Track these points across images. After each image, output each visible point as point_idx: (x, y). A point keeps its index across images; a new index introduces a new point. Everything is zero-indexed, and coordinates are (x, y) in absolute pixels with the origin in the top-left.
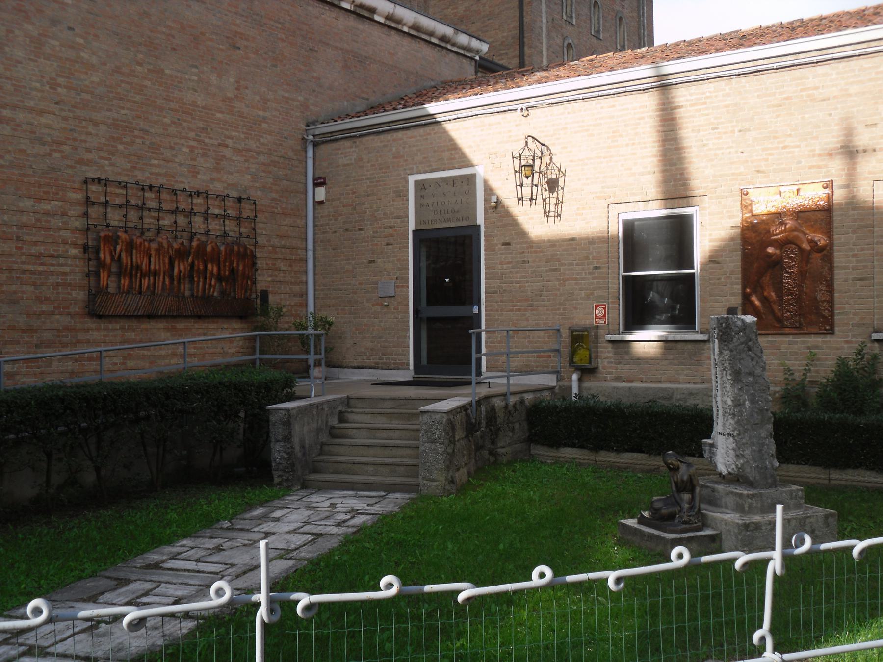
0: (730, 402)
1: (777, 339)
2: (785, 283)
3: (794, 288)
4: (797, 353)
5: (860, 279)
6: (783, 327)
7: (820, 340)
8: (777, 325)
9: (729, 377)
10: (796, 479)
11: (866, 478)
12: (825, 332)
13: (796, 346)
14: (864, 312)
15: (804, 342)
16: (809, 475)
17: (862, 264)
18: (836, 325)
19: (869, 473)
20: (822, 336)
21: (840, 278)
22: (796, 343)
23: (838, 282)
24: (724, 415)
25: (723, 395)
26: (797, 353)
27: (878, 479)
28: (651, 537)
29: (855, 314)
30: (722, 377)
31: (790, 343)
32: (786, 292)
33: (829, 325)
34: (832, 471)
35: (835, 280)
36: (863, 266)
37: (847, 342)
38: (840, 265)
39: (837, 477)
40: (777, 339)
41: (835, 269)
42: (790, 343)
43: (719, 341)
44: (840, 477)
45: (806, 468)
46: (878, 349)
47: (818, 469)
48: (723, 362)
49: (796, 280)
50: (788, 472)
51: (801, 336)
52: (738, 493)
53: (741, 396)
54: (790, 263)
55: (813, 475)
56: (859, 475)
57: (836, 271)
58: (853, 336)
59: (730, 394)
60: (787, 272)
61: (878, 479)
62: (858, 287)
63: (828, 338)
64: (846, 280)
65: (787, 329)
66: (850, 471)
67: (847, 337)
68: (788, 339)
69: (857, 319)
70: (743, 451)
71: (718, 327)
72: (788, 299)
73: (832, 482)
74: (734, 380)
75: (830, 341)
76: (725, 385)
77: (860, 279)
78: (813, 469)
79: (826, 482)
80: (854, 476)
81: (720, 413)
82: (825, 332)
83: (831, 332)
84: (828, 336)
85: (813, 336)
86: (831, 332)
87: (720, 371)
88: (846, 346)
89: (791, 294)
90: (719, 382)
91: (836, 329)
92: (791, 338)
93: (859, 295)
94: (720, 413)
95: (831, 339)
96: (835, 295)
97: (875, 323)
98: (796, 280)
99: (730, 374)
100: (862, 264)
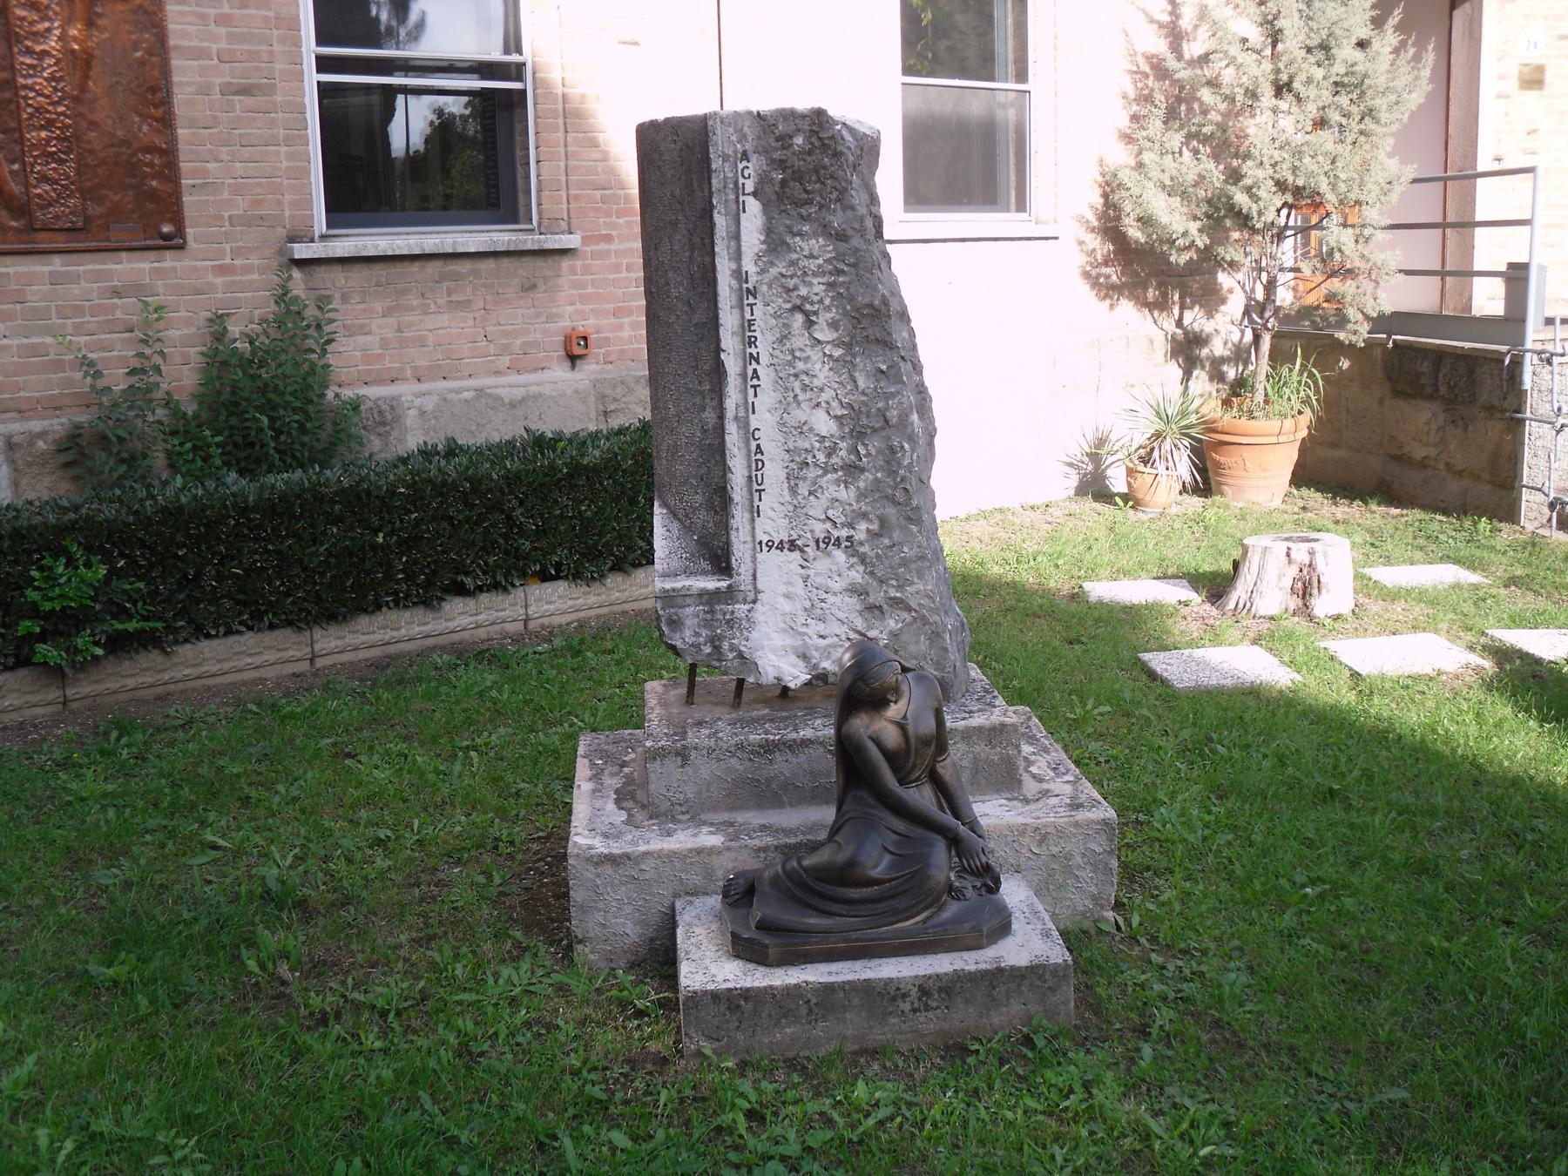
0: (824, 425)
1: (11, 270)
2: (25, 87)
3: (58, 103)
4: (80, 311)
5: (244, 91)
6: (31, 228)
7: (146, 266)
8: (14, 224)
9: (824, 334)
10: (210, 682)
11: (403, 631)
12: (162, 243)
13: (75, 290)
14: (259, 185)
15: (98, 276)
16: (258, 660)
17: (244, 47)
18: (187, 222)
19: (407, 614)
20: (152, 255)
21: (189, 84)
22: (74, 279)
23: (182, 97)
24: (793, 480)
25: (788, 402)
26: (80, 311)
27: (430, 627)
28: (828, 998)
29: (235, 190)
30: (783, 339)
31: (55, 279)
32: (31, 116)
33: (170, 221)
34: (318, 633)
35: (176, 90)
36: (249, 52)
37: (222, 270)
38: (184, 43)
39: (333, 644)
40: (11, 270)
41: (172, 54)
42: (55, 279)
43: (766, 206)
44: (339, 643)
45: (249, 640)
46: (303, 286)
47: (284, 636)
48: (791, 283)
49: (61, 79)
50: (200, 664)
51: (88, 256)
52: (980, 729)
53: (888, 397)
54: (32, 23)
55: (271, 656)
56: (384, 628)
57: (176, 62)
58: (236, 253)
59: (827, 395)
60: (29, 52)
61: (430, 627)
62: (238, 112)
63: (169, 260)
64: (205, 90)
65: (41, 235)
66: (363, 621)
67: (222, 255)
68: (46, 269)
69: (241, 206)
70: (900, 588)
71: (765, 151)
72: (40, 140)
73: (320, 663)
74: (848, 346)
75: (174, 270)
76: (800, 366)
77: (244, 91)
78: (268, 638)
79: (304, 666)
80: (373, 633)
81: (774, 473)
82: (162, 243)
83: (174, 242)
84: (168, 254)
85: (124, 254)
86: (174, 242)
87: (775, 316)
88: (219, 280)
89: (49, 124)
90: (764, 359)
91: (190, 231)
92: (57, 264)
93: (240, 135)
94: (774, 473)
95: (177, 264)
96: (180, 131)
97: (287, 213)
98: (61, 79)
99: (834, 325)
100: (244, 47)
